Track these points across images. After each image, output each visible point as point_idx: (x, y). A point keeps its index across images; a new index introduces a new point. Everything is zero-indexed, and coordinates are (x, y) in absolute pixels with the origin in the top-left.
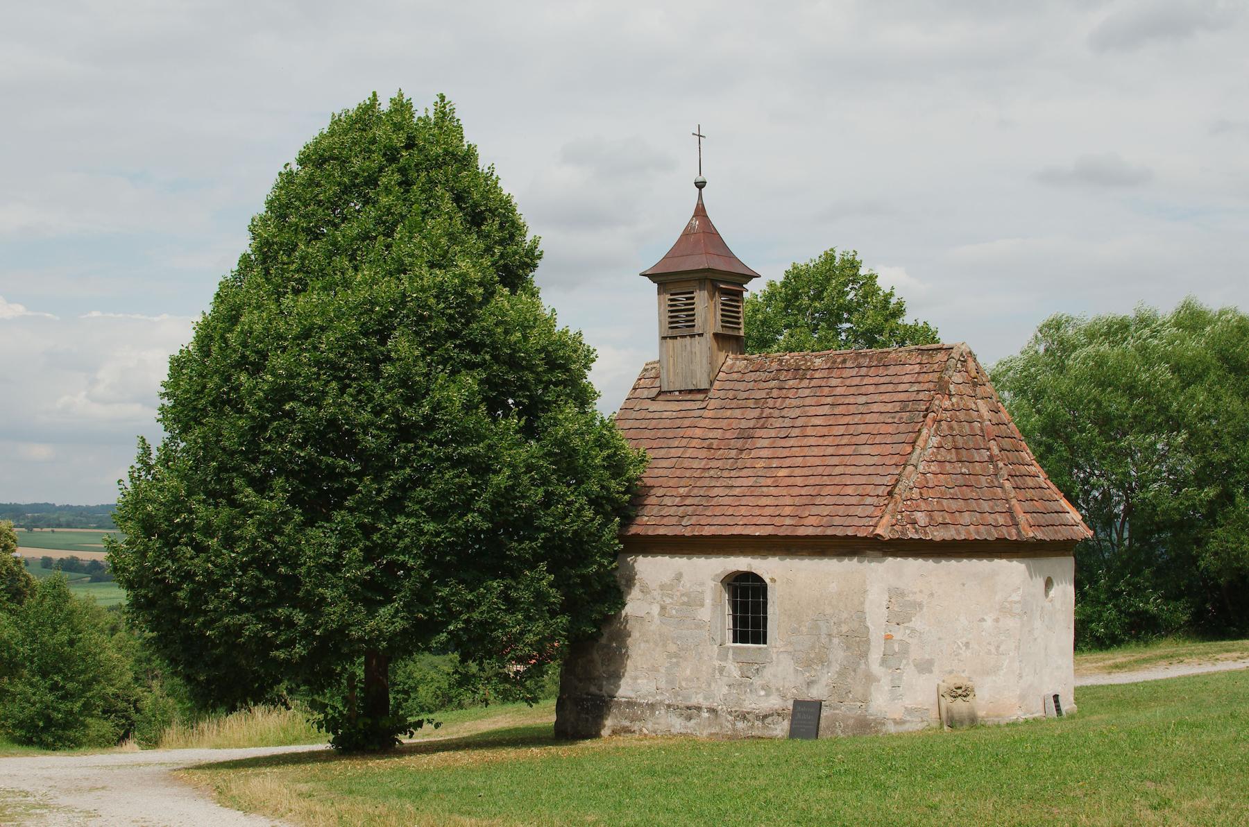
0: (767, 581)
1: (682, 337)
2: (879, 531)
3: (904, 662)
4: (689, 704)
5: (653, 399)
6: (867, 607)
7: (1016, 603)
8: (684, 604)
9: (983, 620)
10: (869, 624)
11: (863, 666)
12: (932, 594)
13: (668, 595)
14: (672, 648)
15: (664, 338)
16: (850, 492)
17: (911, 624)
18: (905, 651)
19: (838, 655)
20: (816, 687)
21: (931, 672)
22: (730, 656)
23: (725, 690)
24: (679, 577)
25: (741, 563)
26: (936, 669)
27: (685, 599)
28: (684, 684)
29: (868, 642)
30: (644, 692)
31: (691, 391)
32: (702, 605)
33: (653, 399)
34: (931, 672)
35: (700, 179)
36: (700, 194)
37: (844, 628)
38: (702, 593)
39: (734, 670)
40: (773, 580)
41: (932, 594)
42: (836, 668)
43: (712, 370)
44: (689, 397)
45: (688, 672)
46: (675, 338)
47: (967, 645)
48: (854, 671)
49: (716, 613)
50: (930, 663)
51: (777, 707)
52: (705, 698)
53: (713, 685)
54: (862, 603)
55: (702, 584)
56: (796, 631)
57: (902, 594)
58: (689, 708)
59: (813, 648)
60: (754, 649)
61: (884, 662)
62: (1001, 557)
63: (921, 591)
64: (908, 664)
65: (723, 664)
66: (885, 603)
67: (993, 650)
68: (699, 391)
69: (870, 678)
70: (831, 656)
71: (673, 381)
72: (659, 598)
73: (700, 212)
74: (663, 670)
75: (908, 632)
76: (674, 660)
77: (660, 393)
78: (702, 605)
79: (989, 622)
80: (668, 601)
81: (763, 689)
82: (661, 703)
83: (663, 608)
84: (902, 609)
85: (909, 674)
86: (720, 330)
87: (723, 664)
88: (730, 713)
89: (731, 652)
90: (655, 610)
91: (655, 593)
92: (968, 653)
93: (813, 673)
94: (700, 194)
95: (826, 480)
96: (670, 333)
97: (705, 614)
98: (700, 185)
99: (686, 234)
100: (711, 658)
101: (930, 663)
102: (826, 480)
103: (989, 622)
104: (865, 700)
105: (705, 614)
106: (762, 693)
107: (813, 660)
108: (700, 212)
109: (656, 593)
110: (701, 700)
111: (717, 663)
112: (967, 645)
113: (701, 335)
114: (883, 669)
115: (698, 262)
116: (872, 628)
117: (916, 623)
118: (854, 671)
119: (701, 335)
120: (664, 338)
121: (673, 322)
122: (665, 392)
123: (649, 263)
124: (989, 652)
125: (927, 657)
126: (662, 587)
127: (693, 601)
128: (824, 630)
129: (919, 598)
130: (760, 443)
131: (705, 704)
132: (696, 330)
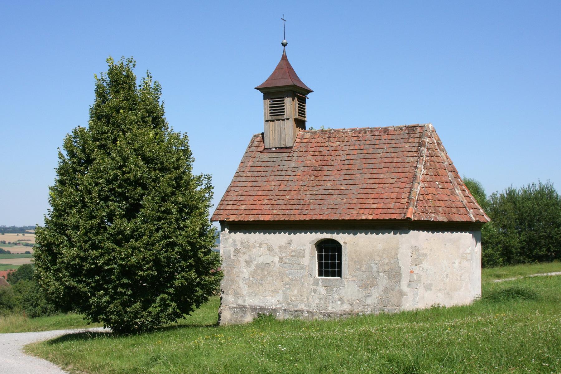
0: (342, 243)
1: (277, 120)
2: (409, 215)
3: (419, 285)
4: (296, 309)
5: (261, 152)
6: (399, 256)
7: (469, 254)
8: (293, 256)
9: (454, 263)
10: (400, 265)
11: (397, 288)
12: (431, 249)
13: (284, 252)
14: (287, 280)
15: (267, 121)
16: (385, 197)
17: (422, 265)
18: (419, 280)
19: (384, 281)
20: (370, 298)
21: (431, 290)
22: (320, 283)
23: (317, 301)
24: (290, 243)
25: (327, 236)
26: (433, 288)
27: (293, 254)
28: (293, 298)
29: (400, 275)
30: (269, 303)
31: (282, 148)
32: (304, 257)
33: (261, 152)
34: (431, 290)
35: (285, 41)
36: (284, 50)
37: (387, 268)
38: (304, 250)
39: (322, 290)
40: (345, 243)
41: (431, 249)
42: (382, 288)
43: (294, 137)
44: (281, 151)
45: (296, 292)
46: (273, 121)
47: (447, 275)
48: (393, 290)
49: (311, 260)
50: (431, 285)
51: (347, 310)
52: (306, 306)
53: (310, 299)
54: (397, 254)
55: (303, 245)
56: (359, 270)
57: (418, 250)
58: (296, 311)
59: (368, 279)
60: (334, 280)
61: (409, 285)
62: (423, 231)
63: (426, 248)
64: (421, 286)
65: (316, 287)
66: (410, 254)
67: (459, 278)
68: (287, 148)
69: (401, 294)
70: (379, 282)
71: (270, 142)
72: (278, 253)
73: (284, 58)
74: (281, 291)
75: (421, 269)
76: (287, 286)
77: (265, 149)
78: (304, 257)
79: (457, 264)
80: (284, 255)
81: (339, 300)
82: (280, 308)
83: (281, 258)
84: (418, 258)
85: (421, 291)
86: (297, 117)
87: (316, 287)
88: (321, 313)
89: (321, 281)
90: (277, 259)
91: (276, 251)
92: (448, 280)
93: (369, 292)
94: (284, 50)
95: (370, 191)
96: (270, 118)
97: (306, 261)
98: (284, 45)
99: (278, 68)
100: (309, 285)
101: (431, 285)
102: (370, 191)
103: (457, 264)
104: (399, 305)
105: (306, 261)
106: (339, 302)
107: (366, 286)
108: (284, 58)
109: (277, 251)
110: (303, 307)
111: (312, 287)
112: (447, 275)
113: (288, 119)
114: (409, 289)
115: (287, 82)
116: (402, 267)
117: (425, 264)
118: (393, 290)
119: (288, 119)
120: (267, 121)
121: (273, 114)
122: (267, 149)
123: (259, 84)
124: (457, 280)
125: (429, 282)
126: (280, 248)
127: (299, 255)
128: (375, 269)
129: (425, 251)
130: (326, 173)
131: (305, 309)
132: (285, 117)
